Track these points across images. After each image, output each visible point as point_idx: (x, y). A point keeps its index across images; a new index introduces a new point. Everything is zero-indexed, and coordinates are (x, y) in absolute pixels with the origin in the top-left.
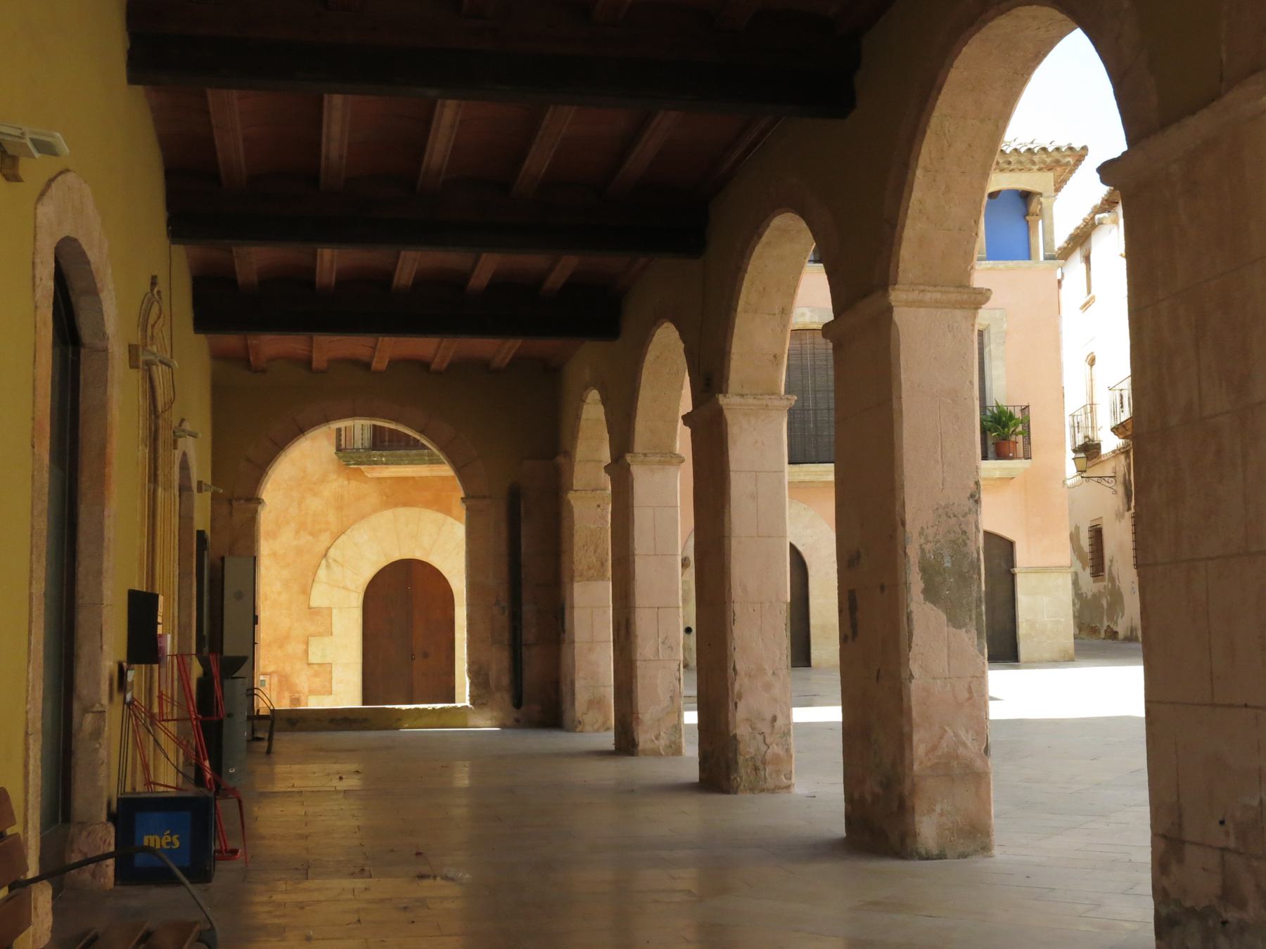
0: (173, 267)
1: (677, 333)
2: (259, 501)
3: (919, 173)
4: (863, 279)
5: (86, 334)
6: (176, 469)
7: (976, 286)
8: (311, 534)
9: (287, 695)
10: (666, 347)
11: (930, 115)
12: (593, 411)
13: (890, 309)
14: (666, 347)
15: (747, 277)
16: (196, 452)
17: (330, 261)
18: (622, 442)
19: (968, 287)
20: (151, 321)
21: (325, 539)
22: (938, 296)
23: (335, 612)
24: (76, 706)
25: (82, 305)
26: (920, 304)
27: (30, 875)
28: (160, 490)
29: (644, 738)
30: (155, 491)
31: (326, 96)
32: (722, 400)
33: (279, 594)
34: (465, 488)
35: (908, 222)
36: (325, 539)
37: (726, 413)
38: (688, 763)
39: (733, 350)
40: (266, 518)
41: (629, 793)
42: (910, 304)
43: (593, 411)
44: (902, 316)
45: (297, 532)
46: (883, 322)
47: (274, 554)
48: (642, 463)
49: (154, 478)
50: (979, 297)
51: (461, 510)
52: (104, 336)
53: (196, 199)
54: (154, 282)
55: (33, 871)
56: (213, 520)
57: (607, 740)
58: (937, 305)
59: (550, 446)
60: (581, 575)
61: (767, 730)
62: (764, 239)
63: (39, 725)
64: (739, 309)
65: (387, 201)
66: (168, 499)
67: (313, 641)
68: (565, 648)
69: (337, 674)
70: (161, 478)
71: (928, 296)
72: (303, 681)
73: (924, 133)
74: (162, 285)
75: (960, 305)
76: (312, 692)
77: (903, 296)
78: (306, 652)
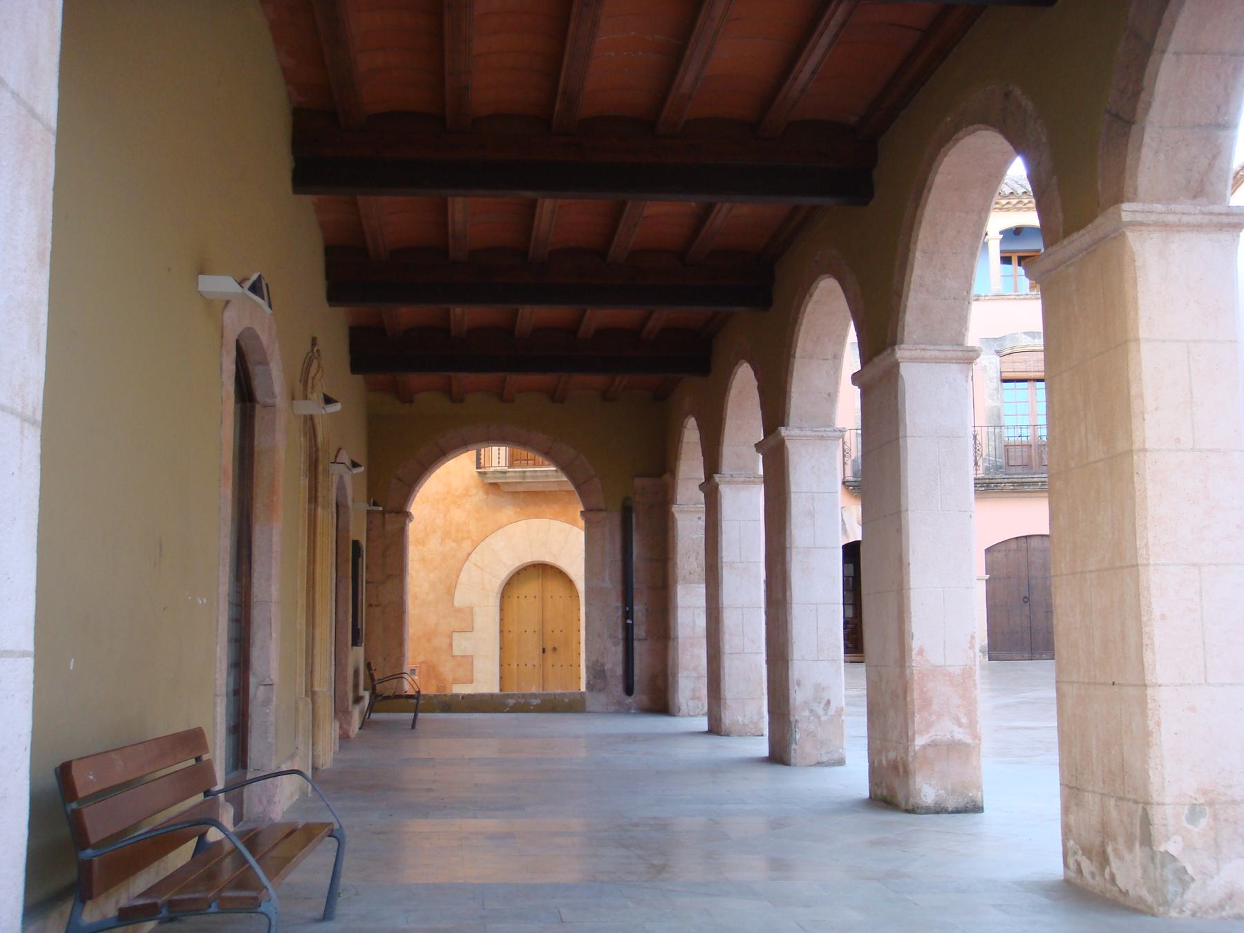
0: (332, 327)
1: (752, 373)
2: (407, 515)
3: (918, 254)
4: (879, 338)
5: (259, 393)
6: (334, 490)
7: (970, 344)
8: (454, 541)
9: (434, 682)
10: (744, 382)
11: (924, 208)
12: (691, 434)
13: (896, 365)
14: (744, 382)
15: (803, 329)
16: (347, 479)
17: (464, 315)
18: (712, 464)
19: (962, 345)
20: (311, 375)
21: (467, 545)
22: (937, 353)
23: (476, 609)
24: (253, 681)
25: (256, 371)
26: (922, 360)
27: (217, 788)
28: (319, 510)
29: (802, 745)
30: (315, 509)
31: (450, 199)
32: (783, 431)
33: (428, 594)
34: (584, 503)
35: (912, 294)
36: (467, 545)
37: (787, 443)
38: (855, 777)
39: (793, 389)
40: (413, 529)
41: (718, 769)
42: (913, 360)
43: (691, 434)
44: (908, 372)
45: (443, 540)
46: (892, 373)
47: (423, 559)
48: (729, 482)
49: (313, 498)
50: (972, 354)
51: (582, 523)
52: (273, 395)
53: (351, 272)
54: (314, 342)
55: (220, 785)
56: (369, 531)
57: (703, 724)
58: (937, 360)
59: (662, 467)
60: (684, 578)
61: (820, 712)
62: (815, 298)
63: (224, 689)
64: (797, 355)
65: (507, 272)
66: (325, 517)
67: (455, 635)
68: (671, 643)
69: (479, 664)
70: (320, 499)
71: (928, 354)
72: (447, 670)
73: (920, 222)
74: (321, 344)
75: (958, 361)
76: (456, 681)
77: (907, 354)
78: (451, 645)
